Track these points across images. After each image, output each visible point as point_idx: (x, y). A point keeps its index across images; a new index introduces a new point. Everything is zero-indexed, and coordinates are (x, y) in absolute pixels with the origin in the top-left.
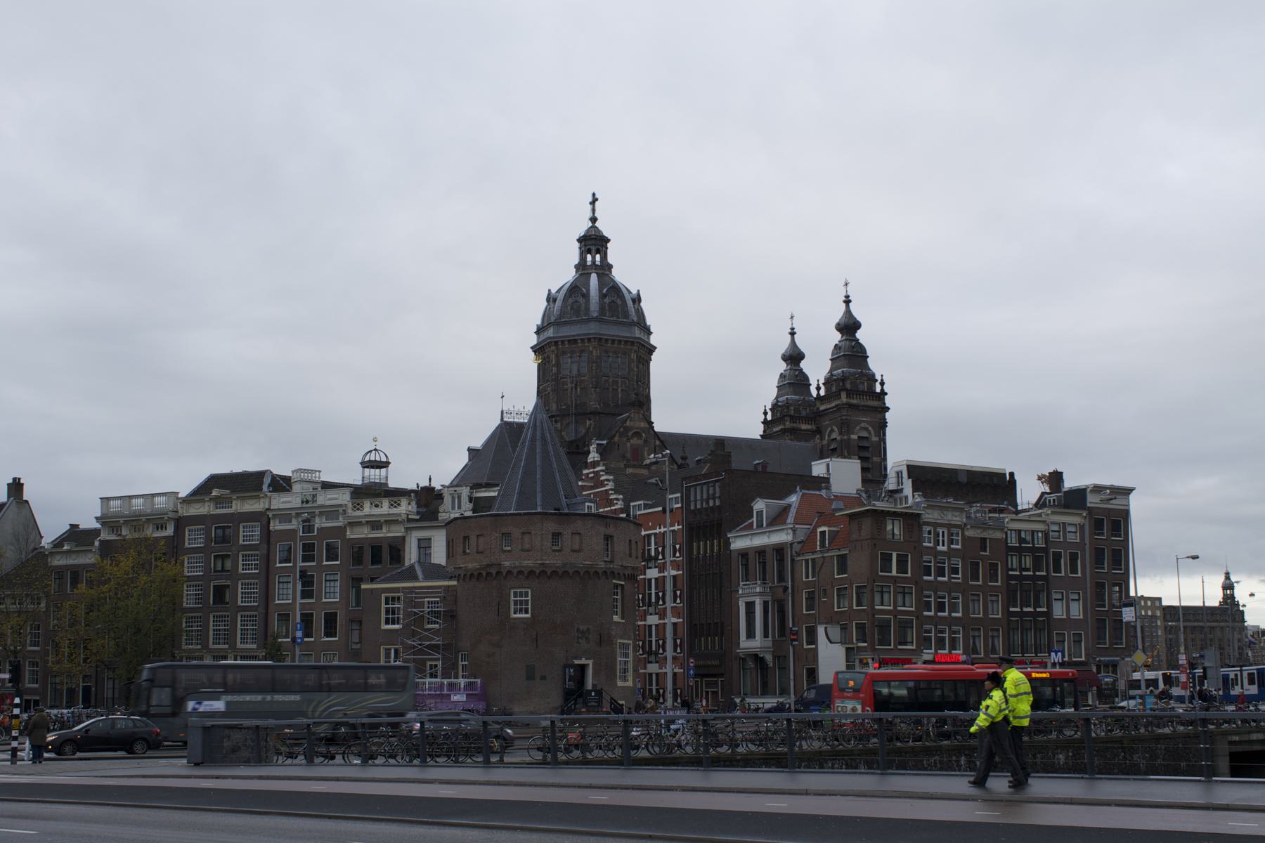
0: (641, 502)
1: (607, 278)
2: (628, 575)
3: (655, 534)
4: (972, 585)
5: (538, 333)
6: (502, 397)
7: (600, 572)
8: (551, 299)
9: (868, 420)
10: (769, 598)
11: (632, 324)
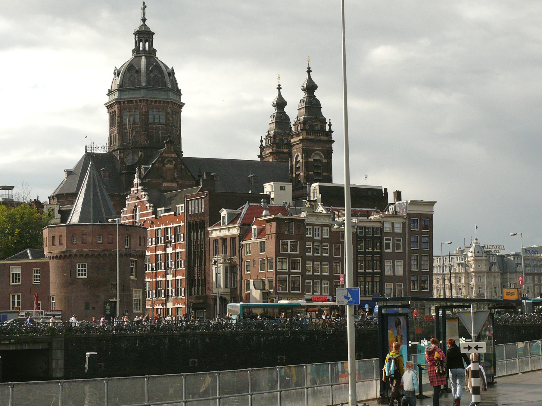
0: (163, 208)
1: (152, 59)
2: (139, 255)
3: (170, 227)
4: (335, 258)
5: (108, 94)
6: (86, 137)
7: (123, 254)
8: (117, 73)
9: (321, 149)
10: (228, 265)
11: (168, 90)
